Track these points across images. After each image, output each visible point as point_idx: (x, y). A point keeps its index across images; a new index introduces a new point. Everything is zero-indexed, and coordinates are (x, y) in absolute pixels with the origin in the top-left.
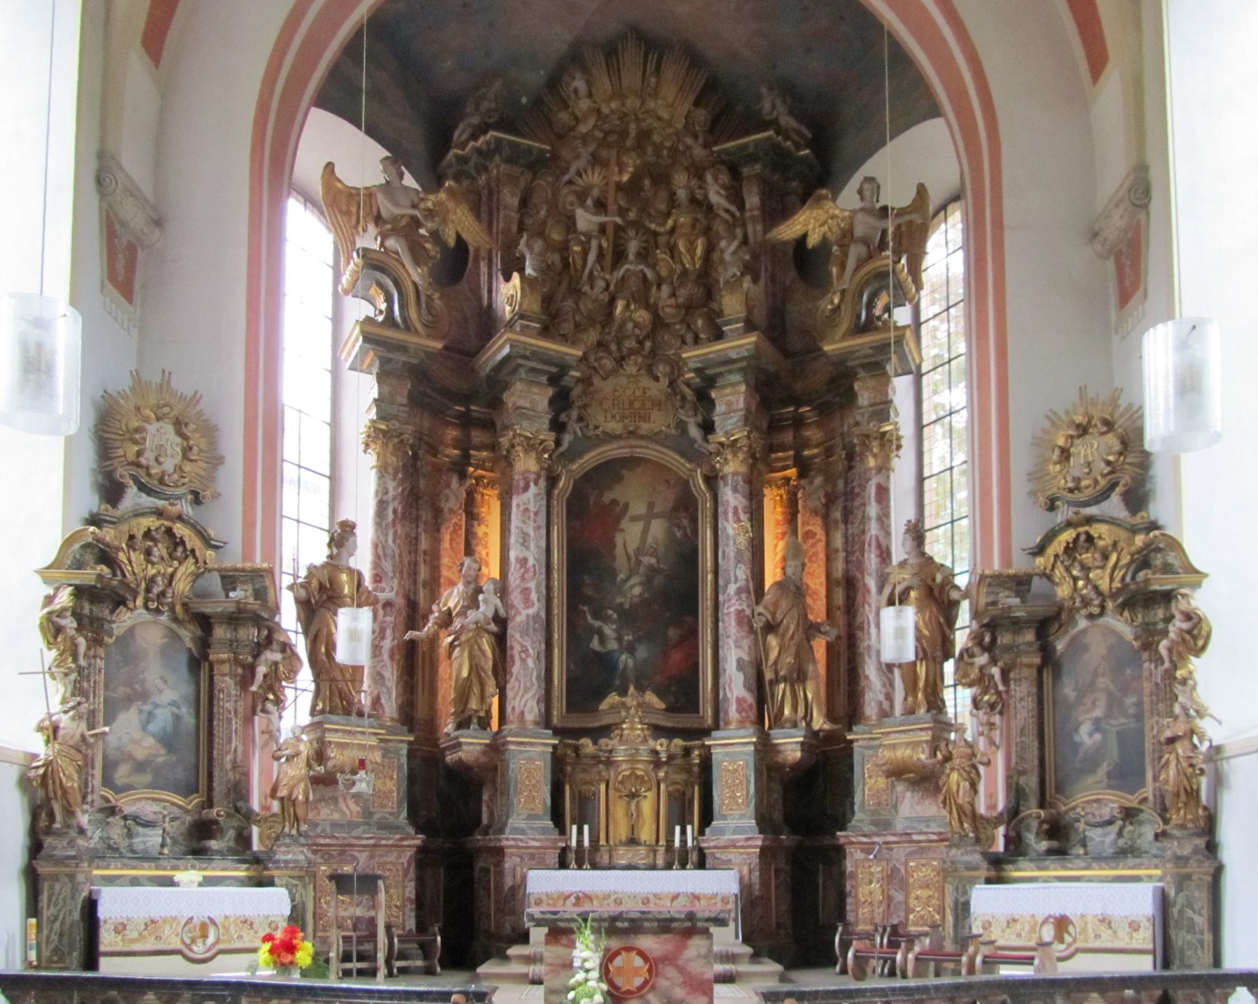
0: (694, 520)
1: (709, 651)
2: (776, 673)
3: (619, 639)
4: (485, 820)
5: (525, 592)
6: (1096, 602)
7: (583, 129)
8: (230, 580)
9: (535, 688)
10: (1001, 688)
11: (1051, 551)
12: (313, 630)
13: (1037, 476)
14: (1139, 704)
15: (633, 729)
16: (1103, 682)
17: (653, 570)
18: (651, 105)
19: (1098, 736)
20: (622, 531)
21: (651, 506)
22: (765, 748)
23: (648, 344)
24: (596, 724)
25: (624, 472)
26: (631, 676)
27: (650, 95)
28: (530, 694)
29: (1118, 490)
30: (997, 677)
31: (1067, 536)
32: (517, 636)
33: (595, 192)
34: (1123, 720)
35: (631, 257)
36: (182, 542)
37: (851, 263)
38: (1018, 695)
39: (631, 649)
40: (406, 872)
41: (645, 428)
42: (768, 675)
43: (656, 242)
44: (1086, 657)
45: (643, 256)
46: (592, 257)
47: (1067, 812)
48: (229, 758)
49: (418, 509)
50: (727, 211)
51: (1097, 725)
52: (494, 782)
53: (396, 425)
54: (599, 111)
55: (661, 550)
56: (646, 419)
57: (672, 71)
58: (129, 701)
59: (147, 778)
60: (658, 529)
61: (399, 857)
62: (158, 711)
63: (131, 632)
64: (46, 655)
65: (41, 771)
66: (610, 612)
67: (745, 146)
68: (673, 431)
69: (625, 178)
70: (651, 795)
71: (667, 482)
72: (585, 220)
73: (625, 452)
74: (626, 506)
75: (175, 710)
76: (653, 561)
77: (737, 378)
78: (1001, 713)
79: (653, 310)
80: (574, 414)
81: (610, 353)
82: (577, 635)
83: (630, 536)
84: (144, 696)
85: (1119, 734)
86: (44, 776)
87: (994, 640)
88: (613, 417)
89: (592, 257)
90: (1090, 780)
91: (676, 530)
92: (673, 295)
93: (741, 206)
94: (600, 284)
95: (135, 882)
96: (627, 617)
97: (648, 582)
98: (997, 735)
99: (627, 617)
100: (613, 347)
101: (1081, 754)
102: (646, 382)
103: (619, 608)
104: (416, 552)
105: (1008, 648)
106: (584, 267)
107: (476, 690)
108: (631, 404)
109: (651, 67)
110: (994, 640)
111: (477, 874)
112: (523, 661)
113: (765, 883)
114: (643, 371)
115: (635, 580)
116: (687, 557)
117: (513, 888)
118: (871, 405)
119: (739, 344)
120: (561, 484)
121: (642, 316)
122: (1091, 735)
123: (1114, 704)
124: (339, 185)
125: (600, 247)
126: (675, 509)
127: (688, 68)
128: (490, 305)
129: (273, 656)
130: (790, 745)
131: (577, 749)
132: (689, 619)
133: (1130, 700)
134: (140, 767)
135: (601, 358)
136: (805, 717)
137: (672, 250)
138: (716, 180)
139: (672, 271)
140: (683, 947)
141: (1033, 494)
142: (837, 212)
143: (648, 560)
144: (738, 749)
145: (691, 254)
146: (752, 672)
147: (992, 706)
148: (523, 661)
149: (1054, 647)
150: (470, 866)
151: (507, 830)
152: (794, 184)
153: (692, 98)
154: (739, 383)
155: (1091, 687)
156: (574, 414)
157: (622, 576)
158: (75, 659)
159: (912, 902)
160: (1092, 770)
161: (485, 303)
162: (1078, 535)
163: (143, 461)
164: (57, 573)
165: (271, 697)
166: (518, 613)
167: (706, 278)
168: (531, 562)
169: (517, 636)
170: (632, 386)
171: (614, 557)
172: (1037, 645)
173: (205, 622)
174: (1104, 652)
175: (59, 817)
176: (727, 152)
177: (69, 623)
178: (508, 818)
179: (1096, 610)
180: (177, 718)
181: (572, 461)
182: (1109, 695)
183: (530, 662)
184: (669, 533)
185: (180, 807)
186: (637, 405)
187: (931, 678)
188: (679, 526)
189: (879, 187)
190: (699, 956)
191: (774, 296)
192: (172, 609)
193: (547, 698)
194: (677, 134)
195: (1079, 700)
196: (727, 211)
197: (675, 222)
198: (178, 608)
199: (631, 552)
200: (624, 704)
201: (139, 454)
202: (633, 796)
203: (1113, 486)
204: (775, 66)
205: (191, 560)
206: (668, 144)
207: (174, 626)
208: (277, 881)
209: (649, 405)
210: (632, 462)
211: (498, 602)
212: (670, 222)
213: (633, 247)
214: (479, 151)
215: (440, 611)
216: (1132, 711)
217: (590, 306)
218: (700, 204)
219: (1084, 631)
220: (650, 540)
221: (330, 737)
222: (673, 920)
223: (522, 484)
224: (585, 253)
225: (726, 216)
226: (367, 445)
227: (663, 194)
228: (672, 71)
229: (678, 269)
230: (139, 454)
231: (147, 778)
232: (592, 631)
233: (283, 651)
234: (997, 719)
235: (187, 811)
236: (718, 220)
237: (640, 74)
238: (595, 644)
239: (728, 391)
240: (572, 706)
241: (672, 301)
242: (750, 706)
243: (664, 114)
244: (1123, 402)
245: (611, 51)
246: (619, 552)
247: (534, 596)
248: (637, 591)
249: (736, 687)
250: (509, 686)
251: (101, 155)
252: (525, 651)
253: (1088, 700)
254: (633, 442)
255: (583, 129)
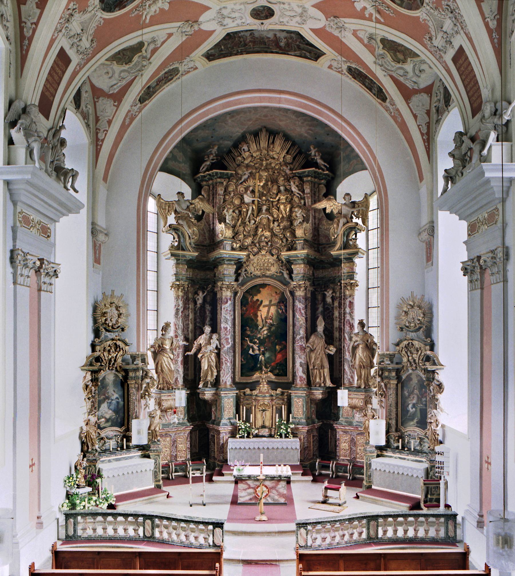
0: (286, 306)
1: (291, 345)
2: (314, 367)
3: (259, 350)
4: (213, 418)
5: (227, 339)
6: (414, 366)
7: (246, 162)
8: (134, 358)
9: (230, 373)
10: (384, 390)
11: (401, 346)
12: (156, 361)
13: (398, 318)
14: (426, 401)
15: (264, 387)
16: (416, 391)
17: (271, 325)
18: (271, 153)
19: (414, 409)
20: (261, 311)
21: (271, 301)
22: (310, 394)
23: (270, 243)
24: (251, 381)
25: (261, 289)
26: (263, 363)
27: (271, 150)
28: (228, 375)
29: (422, 329)
30: (383, 386)
31: (406, 343)
32: (224, 355)
33: (251, 189)
34: (421, 405)
35: (264, 211)
36: (119, 346)
37: (341, 224)
38: (390, 393)
39: (264, 354)
40: (187, 439)
41: (268, 273)
42: (311, 367)
43: (273, 205)
44: (411, 382)
45: (268, 210)
46: (250, 212)
47: (404, 432)
48: (134, 415)
49: (189, 304)
50: (298, 193)
51: (414, 406)
52: (216, 405)
53: (182, 282)
54: (252, 156)
55: (274, 317)
56: (269, 270)
57: (278, 142)
58: (104, 400)
59: (110, 424)
60: (273, 310)
61: (184, 434)
62: (113, 401)
63: (104, 378)
64: (83, 395)
65: (85, 434)
66: (256, 340)
67: (305, 172)
68: (279, 274)
69: (262, 184)
70: (270, 410)
71: (276, 292)
72: (248, 199)
73: (262, 282)
74: (262, 302)
75: (117, 400)
76: (271, 321)
77: (301, 262)
78: (385, 397)
79: (271, 230)
80: (244, 270)
81: (256, 246)
82: (244, 351)
83: (263, 312)
84: (108, 398)
85: (420, 409)
86: (86, 436)
87: (382, 373)
88: (257, 269)
89: (250, 212)
90: (412, 423)
91: (279, 310)
92: (279, 226)
93: (303, 192)
94: (253, 222)
95: (109, 461)
96: (262, 342)
97: (269, 329)
98: (383, 405)
99: (262, 342)
100: (257, 245)
101: (409, 415)
102: (269, 257)
103: (259, 339)
104: (188, 320)
105: (387, 377)
106: (247, 215)
107: (210, 373)
108: (264, 265)
109: (271, 141)
110: (382, 373)
111: (210, 437)
112: (226, 364)
113: (309, 442)
114: (268, 253)
115: (265, 328)
116: (283, 320)
117: (223, 444)
118: (348, 273)
119: (301, 252)
120: (239, 295)
121: (268, 234)
122: (412, 408)
123: (419, 399)
124: (162, 201)
125: (253, 208)
126: (279, 303)
127: (284, 141)
128: (213, 229)
129: (148, 380)
130: (318, 394)
131: (244, 393)
132: (284, 342)
133: (424, 399)
134: (107, 421)
135: (252, 248)
136: (323, 382)
137: (278, 209)
138: (294, 183)
139: (278, 216)
140: (277, 485)
141: (396, 324)
142: (337, 203)
143: (269, 321)
144: (300, 395)
145: (284, 209)
146: (305, 367)
147: (382, 395)
148: (226, 364)
149: (402, 377)
150: (208, 434)
151: (221, 424)
152: (323, 181)
153: (285, 151)
154: (301, 264)
155: (412, 392)
156: (244, 270)
157: (260, 327)
158: (91, 394)
159: (358, 451)
160: (412, 420)
161: (212, 228)
162: (409, 343)
163: (107, 322)
164: (85, 368)
165: (147, 394)
166: (224, 347)
167: (290, 219)
168: (229, 328)
169: (224, 355)
170: (264, 258)
171: (257, 320)
172: (396, 377)
173: (126, 371)
174: (416, 382)
175: (90, 447)
176: (298, 173)
177: (90, 384)
178: (221, 419)
179: (414, 368)
180: (118, 403)
181: (242, 286)
182: (418, 396)
183: (228, 364)
184: (277, 311)
185: (119, 431)
186: (266, 265)
187: (366, 375)
188: (281, 309)
189: (351, 197)
190: (282, 487)
191: (315, 224)
192: (116, 368)
193: (234, 372)
194: (280, 164)
195: (409, 396)
196: (298, 193)
197: (279, 198)
198: (118, 368)
199: (263, 318)
200: (261, 377)
201: (106, 320)
202: (264, 411)
203: (420, 328)
204: (316, 138)
205: (122, 351)
206: (277, 167)
207: (117, 373)
208: (151, 456)
209: (270, 265)
210: (264, 286)
211: (218, 342)
212: (277, 198)
213: (264, 208)
214: (209, 175)
215: (197, 344)
216: (424, 403)
217: (249, 229)
218: (288, 191)
219: (411, 374)
220: (270, 314)
221: (163, 398)
222: (275, 477)
223: (225, 300)
224: (248, 211)
225: (298, 195)
226: (172, 287)
227: (275, 187)
228: (278, 142)
229: (281, 216)
230: (106, 320)
231: (110, 424)
232: (249, 347)
233: (151, 378)
234: (383, 399)
235: (121, 432)
236: (295, 197)
237: (267, 143)
238: (251, 352)
239: (298, 266)
240: (242, 375)
241: (278, 228)
242: (304, 379)
243: (276, 156)
244: (426, 297)
245: (256, 135)
246: (259, 319)
247: (230, 341)
248: (266, 332)
249: (300, 373)
250: (221, 372)
251: (93, 224)
252: (227, 360)
253: (412, 397)
254: (264, 279)
255: (246, 162)
